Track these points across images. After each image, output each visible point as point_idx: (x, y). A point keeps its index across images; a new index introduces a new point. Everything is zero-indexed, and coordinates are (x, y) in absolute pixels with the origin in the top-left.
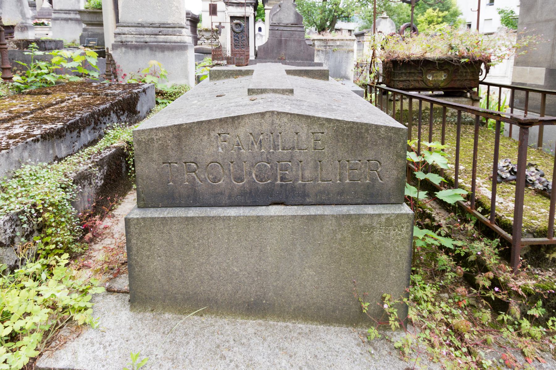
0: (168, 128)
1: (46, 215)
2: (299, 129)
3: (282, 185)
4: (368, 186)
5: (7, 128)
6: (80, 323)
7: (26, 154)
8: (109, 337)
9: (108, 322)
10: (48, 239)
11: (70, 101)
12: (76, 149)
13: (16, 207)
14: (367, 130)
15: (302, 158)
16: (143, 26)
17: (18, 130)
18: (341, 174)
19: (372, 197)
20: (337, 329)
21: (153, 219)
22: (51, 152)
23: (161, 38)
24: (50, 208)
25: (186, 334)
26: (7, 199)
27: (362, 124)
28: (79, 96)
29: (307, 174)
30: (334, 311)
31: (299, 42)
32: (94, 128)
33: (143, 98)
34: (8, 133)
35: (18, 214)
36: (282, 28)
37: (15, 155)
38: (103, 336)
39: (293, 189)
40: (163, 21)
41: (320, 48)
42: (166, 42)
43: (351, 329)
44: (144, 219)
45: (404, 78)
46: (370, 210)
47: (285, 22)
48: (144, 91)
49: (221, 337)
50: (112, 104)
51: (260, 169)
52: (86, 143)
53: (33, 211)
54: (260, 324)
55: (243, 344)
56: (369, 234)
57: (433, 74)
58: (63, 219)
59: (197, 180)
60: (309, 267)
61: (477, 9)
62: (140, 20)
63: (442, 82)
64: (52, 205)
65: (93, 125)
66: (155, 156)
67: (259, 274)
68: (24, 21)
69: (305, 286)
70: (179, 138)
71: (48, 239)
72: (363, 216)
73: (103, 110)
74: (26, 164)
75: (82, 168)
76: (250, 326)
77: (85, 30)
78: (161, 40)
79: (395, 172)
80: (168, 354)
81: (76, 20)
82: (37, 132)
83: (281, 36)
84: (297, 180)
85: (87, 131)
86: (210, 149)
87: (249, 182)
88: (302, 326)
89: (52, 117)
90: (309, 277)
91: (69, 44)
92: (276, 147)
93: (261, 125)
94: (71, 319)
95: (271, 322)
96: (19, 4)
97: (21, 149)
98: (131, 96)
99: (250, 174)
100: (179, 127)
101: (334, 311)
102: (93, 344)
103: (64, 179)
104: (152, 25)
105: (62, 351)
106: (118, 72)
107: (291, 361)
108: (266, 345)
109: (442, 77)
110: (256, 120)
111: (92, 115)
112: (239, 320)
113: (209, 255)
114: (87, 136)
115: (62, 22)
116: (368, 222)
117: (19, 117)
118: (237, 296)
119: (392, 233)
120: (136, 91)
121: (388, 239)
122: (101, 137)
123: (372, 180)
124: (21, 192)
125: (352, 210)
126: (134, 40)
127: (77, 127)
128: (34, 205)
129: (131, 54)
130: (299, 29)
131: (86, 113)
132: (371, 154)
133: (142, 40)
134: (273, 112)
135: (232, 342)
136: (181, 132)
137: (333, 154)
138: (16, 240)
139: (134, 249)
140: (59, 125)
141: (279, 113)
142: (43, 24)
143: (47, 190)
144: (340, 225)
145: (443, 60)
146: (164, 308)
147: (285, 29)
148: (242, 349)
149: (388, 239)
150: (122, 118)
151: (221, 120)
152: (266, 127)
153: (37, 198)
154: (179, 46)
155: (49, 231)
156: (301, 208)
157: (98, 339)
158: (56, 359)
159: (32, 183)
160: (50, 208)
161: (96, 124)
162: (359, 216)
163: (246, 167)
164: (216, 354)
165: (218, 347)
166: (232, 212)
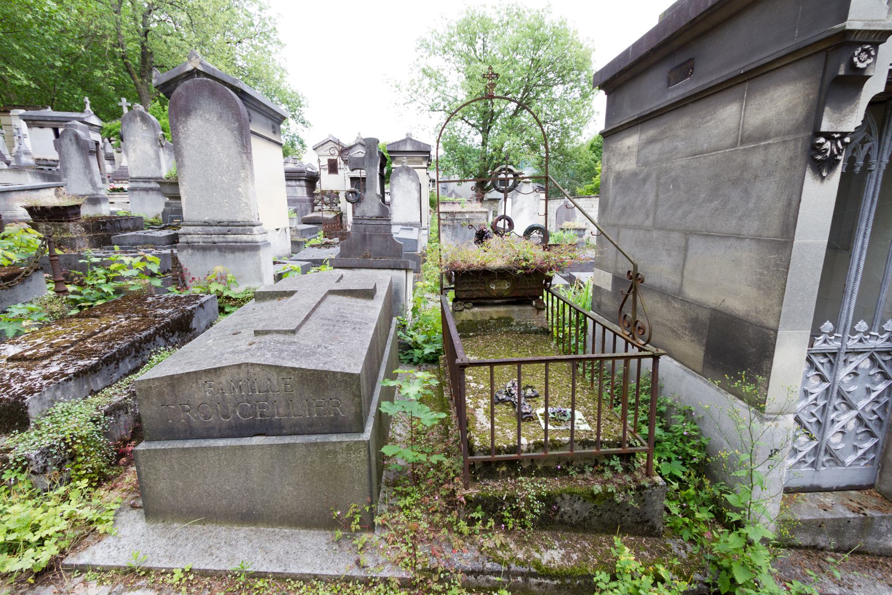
0: (162, 378)
1: (76, 447)
2: (270, 376)
3: (261, 420)
4: (332, 419)
5: (45, 366)
6: (101, 532)
7: (59, 393)
8: (124, 541)
9: (125, 531)
10: (80, 466)
11: (115, 327)
12: (114, 379)
13: (46, 442)
14: (326, 376)
15: (275, 399)
16: (209, 225)
17: (55, 368)
18: (309, 410)
19: (337, 428)
20: (316, 532)
21: (156, 450)
22: (86, 387)
23: (231, 237)
24: (79, 441)
25: (187, 539)
26: (41, 435)
27: (321, 371)
28: (126, 319)
29: (281, 411)
30: (312, 518)
31: (385, 236)
32: (135, 357)
33: (200, 314)
34: (44, 372)
35: (48, 448)
36: (366, 222)
37: (47, 396)
38: (119, 541)
39: (271, 422)
40: (232, 218)
41: (446, 222)
42: (236, 242)
43: (328, 532)
44: (148, 450)
45: (467, 288)
46: (334, 438)
47: (370, 214)
48: (201, 306)
49: (215, 540)
50: (157, 329)
51: (242, 408)
52: (127, 372)
53: (62, 444)
54: (252, 530)
55: (231, 545)
56: (334, 458)
57: (496, 283)
58: (92, 449)
59: (192, 418)
60: (288, 485)
61: (543, 212)
62: (206, 219)
63: (506, 291)
64: (81, 438)
65: (133, 353)
66: (154, 400)
67: (247, 490)
68: (95, 192)
69: (286, 500)
70: (173, 386)
71: (80, 466)
72: (327, 443)
73: (146, 337)
74: (60, 401)
75: (116, 399)
76: (243, 531)
77: (167, 204)
78: (230, 240)
79: (353, 408)
80: (168, 553)
81: (158, 190)
82: (71, 371)
83: (365, 231)
84: (273, 416)
85: (127, 360)
86: (200, 393)
87: (234, 419)
88: (287, 531)
89: (91, 350)
90: (289, 491)
91: (151, 220)
92: (253, 391)
93: (239, 374)
94: (94, 530)
95: (262, 529)
96: (87, 171)
97: (53, 390)
98: (184, 314)
99: (235, 412)
100: (172, 377)
101: (312, 518)
102: (109, 547)
103: (95, 413)
104: (219, 223)
105: (84, 553)
106: (186, 276)
107: (266, 556)
108: (250, 545)
109: (506, 286)
110: (235, 370)
111: (132, 344)
112: (235, 527)
113: (205, 477)
114: (127, 365)
115: (141, 193)
116: (332, 448)
117: (59, 351)
118: (232, 509)
119: (353, 456)
120: (189, 308)
121: (350, 461)
122: (144, 363)
123: (335, 414)
124: (53, 428)
125: (319, 438)
126: (201, 240)
127: (114, 360)
128: (64, 439)
129: (198, 256)
130: (385, 223)
131: (123, 344)
132: (332, 394)
133: (210, 240)
134: (247, 364)
135: (223, 544)
136: (174, 381)
137: (301, 395)
138: (48, 468)
139: (143, 474)
140: (94, 360)
141: (252, 364)
142: (122, 189)
143: (75, 425)
144: (309, 451)
145: (503, 270)
146: (173, 520)
147: (370, 222)
148: (229, 549)
149: (350, 461)
150: (171, 340)
151: (205, 371)
152: (243, 375)
153: (66, 433)
154: (250, 246)
155: (80, 459)
156: (279, 437)
157: (115, 544)
158: (79, 558)
159: (64, 419)
160: (79, 441)
161: (137, 351)
162: (324, 444)
163: (231, 408)
164: (206, 552)
165: (210, 547)
166: (221, 443)
